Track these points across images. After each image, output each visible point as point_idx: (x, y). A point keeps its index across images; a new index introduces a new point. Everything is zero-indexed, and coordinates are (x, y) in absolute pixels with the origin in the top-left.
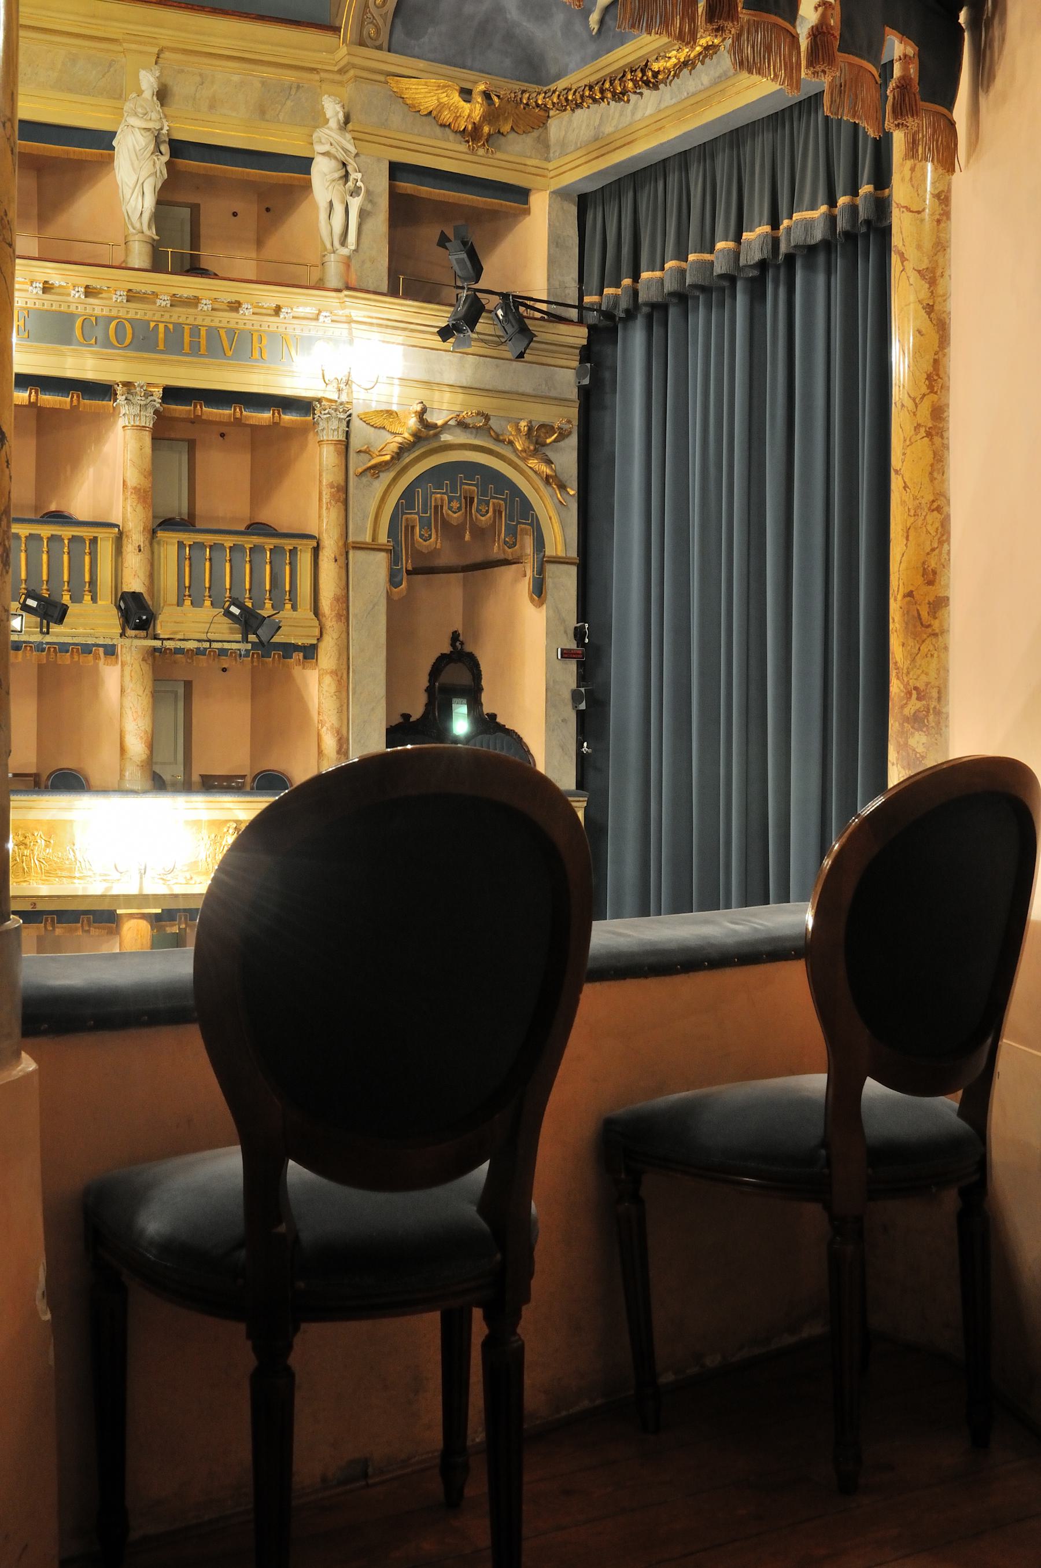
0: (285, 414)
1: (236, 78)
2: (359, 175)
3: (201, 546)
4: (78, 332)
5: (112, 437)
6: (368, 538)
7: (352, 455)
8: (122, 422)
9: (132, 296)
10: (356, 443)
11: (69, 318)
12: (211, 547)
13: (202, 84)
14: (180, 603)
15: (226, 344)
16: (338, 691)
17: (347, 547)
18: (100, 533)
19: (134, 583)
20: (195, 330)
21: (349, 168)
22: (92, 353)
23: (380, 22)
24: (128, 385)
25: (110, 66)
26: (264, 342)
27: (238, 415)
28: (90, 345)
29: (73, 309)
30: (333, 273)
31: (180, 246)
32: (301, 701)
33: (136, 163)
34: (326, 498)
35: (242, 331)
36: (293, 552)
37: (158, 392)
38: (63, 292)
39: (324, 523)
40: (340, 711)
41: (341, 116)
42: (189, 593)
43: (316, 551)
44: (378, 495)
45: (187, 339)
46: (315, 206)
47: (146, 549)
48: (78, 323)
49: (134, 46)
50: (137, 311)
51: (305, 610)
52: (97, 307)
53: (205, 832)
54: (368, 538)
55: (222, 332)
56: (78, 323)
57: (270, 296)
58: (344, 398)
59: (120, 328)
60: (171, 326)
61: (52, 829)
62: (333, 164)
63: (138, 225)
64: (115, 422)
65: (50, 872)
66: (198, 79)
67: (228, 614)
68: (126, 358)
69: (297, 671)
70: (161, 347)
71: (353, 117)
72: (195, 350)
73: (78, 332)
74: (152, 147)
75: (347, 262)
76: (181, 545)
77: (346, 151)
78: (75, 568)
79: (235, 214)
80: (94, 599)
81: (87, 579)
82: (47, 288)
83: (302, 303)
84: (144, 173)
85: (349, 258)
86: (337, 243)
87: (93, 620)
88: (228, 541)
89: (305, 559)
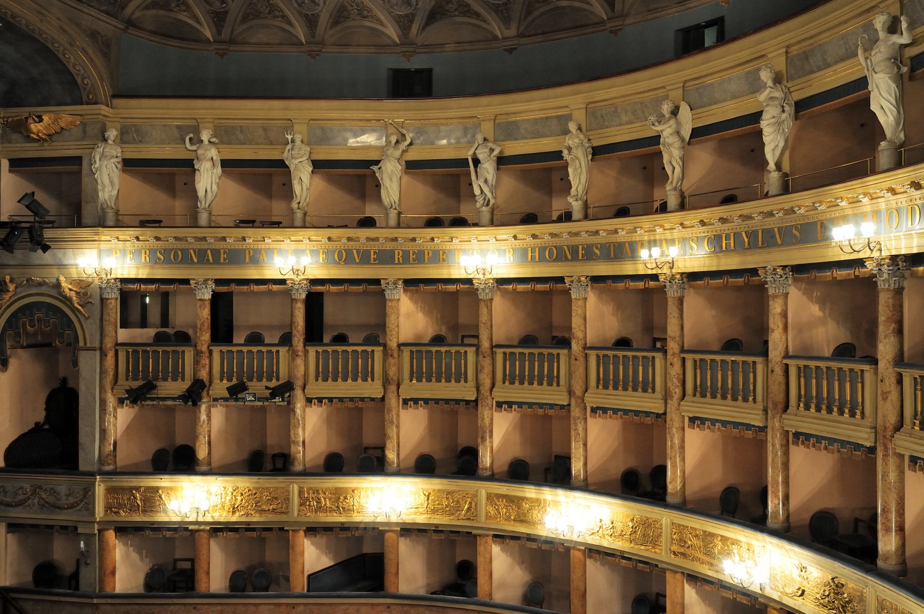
55: (355, 251)
59: (176, 253)
78: (365, 366)
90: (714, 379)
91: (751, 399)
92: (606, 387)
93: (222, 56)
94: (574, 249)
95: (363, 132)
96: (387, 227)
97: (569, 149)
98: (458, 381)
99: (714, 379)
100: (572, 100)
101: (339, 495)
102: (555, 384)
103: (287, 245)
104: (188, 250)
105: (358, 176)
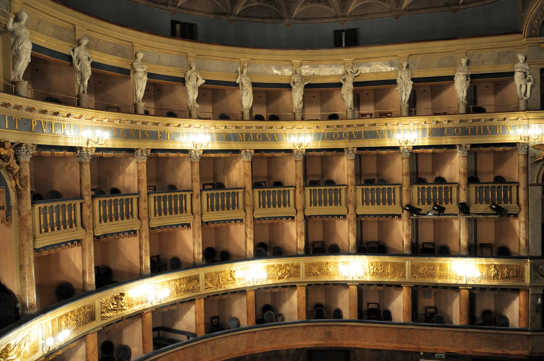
1: (489, 54)
2: (531, 76)
3: (482, 187)
4: (446, 132)
5: (455, 158)
6: (535, 182)
7: (529, 159)
8: (458, 155)
9: (461, 121)
10: (530, 155)
11: (443, 129)
14: (476, 203)
15: (489, 130)
16: (526, 227)
17: (528, 186)
19: (463, 199)
20: (479, 128)
21: (527, 74)
23: (537, 28)
24: (460, 145)
29: (444, 126)
30: (522, 105)
31: (473, 106)
32: (514, 230)
34: (521, 170)
35: (494, 126)
36: (511, 187)
37: (469, 146)
38: (442, 122)
39: (521, 179)
40: (526, 233)
41: (524, 59)
42: (479, 200)
43: (518, 187)
44: (538, 169)
45: (477, 130)
46: (515, 86)
47: (466, 189)
48: (446, 130)
50: (463, 125)
51: (514, 204)
52: (451, 125)
53: (485, 267)
54: (535, 182)
55: (488, 127)
56: (446, 130)
57: (502, 116)
58: (526, 142)
59: (458, 130)
61: (441, 265)
62: (522, 74)
64: (456, 154)
65: (441, 277)
67: (491, 207)
68: (460, 138)
69: (512, 220)
70: (469, 133)
71: (528, 58)
72: (480, 133)
73: (446, 132)
75: (527, 101)
76: (476, 187)
77: (525, 69)
78: (446, 195)
79: (487, 87)
80: (451, 203)
82: (437, 122)
83: (513, 116)
84: (463, 87)
85: (527, 100)
86: (523, 96)
87: (452, 208)
88: (490, 186)
89: (514, 189)
91: (74, 225)
92: (212, 210)
93: (397, 18)
94: (248, 135)
101: (321, 267)
103: (295, 131)
104: (486, 126)
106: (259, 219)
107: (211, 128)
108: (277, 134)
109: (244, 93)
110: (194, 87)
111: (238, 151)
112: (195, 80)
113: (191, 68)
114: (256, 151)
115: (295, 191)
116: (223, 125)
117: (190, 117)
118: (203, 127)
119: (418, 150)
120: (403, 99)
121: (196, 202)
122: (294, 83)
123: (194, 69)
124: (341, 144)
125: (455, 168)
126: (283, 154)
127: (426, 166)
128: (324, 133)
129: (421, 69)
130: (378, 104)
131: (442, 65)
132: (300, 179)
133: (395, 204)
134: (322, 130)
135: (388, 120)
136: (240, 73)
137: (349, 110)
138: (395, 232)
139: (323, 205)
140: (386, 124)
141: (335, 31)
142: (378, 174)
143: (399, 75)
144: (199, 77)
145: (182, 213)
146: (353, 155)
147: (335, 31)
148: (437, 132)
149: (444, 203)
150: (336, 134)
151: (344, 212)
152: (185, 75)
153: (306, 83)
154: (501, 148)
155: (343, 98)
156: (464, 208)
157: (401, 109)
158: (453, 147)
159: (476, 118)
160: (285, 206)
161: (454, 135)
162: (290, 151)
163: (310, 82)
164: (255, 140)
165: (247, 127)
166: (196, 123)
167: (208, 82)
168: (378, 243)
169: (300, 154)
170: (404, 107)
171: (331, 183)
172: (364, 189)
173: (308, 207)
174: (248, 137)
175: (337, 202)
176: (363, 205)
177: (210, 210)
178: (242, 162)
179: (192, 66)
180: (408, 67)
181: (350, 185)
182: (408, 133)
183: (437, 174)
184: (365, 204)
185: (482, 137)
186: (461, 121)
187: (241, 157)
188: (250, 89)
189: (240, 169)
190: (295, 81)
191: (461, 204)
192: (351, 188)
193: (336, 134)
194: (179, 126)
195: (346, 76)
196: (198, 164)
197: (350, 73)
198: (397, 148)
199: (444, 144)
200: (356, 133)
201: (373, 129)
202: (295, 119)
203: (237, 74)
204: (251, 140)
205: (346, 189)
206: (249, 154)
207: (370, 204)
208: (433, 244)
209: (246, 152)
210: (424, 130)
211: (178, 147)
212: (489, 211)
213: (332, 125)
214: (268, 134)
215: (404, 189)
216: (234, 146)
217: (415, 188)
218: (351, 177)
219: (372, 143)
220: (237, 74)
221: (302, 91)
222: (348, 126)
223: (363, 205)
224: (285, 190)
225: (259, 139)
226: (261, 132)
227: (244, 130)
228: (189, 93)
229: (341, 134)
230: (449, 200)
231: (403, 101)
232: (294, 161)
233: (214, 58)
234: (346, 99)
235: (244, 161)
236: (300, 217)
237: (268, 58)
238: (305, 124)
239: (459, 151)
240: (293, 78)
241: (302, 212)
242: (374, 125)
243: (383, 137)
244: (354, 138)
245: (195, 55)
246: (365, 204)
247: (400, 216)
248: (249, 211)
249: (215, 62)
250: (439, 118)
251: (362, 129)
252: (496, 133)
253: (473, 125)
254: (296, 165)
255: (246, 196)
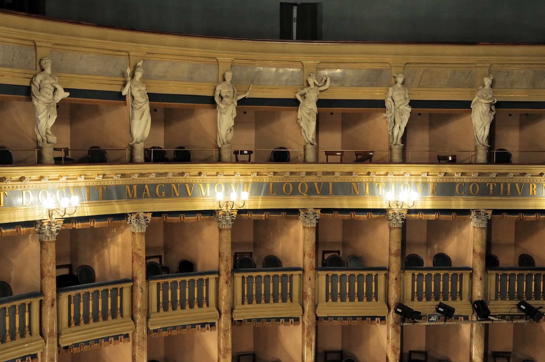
0: (541, 215)
1: (522, 71)
5: (467, 228)
8: (472, 224)
9: (480, 174)
12: (509, 275)
13: (508, 76)
18: (464, 272)
19: (478, 294)
22: (463, 199)
25: (469, 74)
26: (535, 187)
27: (521, 217)
28: (462, 195)
29: (455, 181)
33: (482, 117)
35: (525, 183)
37: (490, 213)
42: (501, 295)
48: (458, 185)
49: (480, 65)
50: (482, 180)
52: (465, 179)
55: (517, 185)
56: (458, 185)
59: (474, 187)
60: (495, 184)
63: (481, 142)
66: (506, 74)
68: (477, 200)
72: (505, 194)
74: (489, 109)
76: (497, 275)
79: (510, 115)
81: (458, 291)
82: (446, 174)
90: (174, 295)
94: (141, 188)
95: (336, 69)
96: (305, 162)
97: (221, 97)
98: (284, 301)
99: (174, 295)
100: (225, 51)
102: (205, 305)
103: (222, 179)
105: (257, 110)
106: (155, 331)
107: (79, 179)
108: (191, 185)
109: (137, 114)
110: (49, 106)
111: (123, 216)
112: (51, 93)
113: (43, 70)
114: (155, 214)
115: (217, 281)
116: (101, 172)
117: (40, 161)
118: (64, 179)
119: (413, 215)
120: (396, 134)
121: (49, 314)
122: (221, 97)
123: (48, 71)
124: (295, 203)
125: (465, 244)
126: (199, 216)
127: (418, 235)
128: (268, 184)
129: (423, 87)
130: (351, 132)
131: (453, 84)
132: (227, 261)
133: (377, 300)
134: (265, 179)
135: (371, 168)
136: (129, 79)
137: (309, 147)
138: (372, 341)
139: (263, 301)
140: (369, 174)
141: (282, 4)
142: (345, 244)
143: (390, 94)
144: (57, 86)
145: (114, 317)
146: (314, 221)
147: (282, 4)
148: (444, 189)
149: (450, 299)
150: (288, 186)
151: (297, 313)
152: (31, 82)
153: (240, 97)
154: (534, 216)
155: (299, 124)
156: (481, 309)
157: (391, 149)
158: (466, 212)
159: (502, 171)
160: (200, 306)
161: (469, 194)
162: (211, 213)
163: (247, 95)
164: (154, 195)
165: (141, 175)
166: (52, 172)
167: (74, 93)
168: (341, 353)
169: (228, 218)
170: (397, 147)
171: (273, 262)
172: (330, 275)
173: (238, 306)
174: (141, 192)
175: (286, 296)
176: (327, 300)
177: (73, 325)
178: (130, 234)
179: (44, 66)
180: (403, 83)
181: (307, 269)
182: (402, 190)
183: (436, 246)
184: (330, 300)
185: (511, 200)
186: (480, 174)
187: (126, 225)
188: (146, 107)
189: (124, 246)
190: (223, 95)
191: (476, 302)
192: (310, 273)
193: (288, 186)
194: (22, 179)
195: (305, 90)
196: (54, 245)
197: (312, 86)
198: (383, 211)
199: (453, 208)
200: (319, 184)
201: (348, 179)
202: (220, 160)
203: (122, 79)
204: (146, 196)
205: (300, 275)
206: (143, 222)
207: (339, 300)
208: (425, 353)
209: (138, 217)
210: (425, 184)
211: (20, 217)
212: (515, 311)
213: (282, 170)
214: (176, 185)
215: (393, 276)
216: (117, 208)
217: (408, 276)
218: (310, 257)
219: (345, 203)
220: (122, 79)
221: (235, 112)
222: (308, 174)
223: (327, 300)
224: (202, 279)
225: (161, 194)
226: (163, 181)
227: (136, 179)
228: (40, 117)
229: (295, 185)
230: (456, 295)
231: (395, 137)
232: (217, 231)
233: (84, 49)
234: (304, 127)
235: (133, 233)
236: (225, 322)
237: (178, 52)
238: (239, 168)
239: (475, 220)
240: (219, 88)
241: (229, 315)
242: (351, 173)
243: (362, 193)
244: (316, 194)
245: (50, 45)
246: (330, 300)
247: (383, 319)
248: (139, 317)
249: (85, 56)
250: (448, 169)
251: (329, 179)
252: (528, 195)
253: (497, 181)
254: (220, 236)
255: (135, 294)
